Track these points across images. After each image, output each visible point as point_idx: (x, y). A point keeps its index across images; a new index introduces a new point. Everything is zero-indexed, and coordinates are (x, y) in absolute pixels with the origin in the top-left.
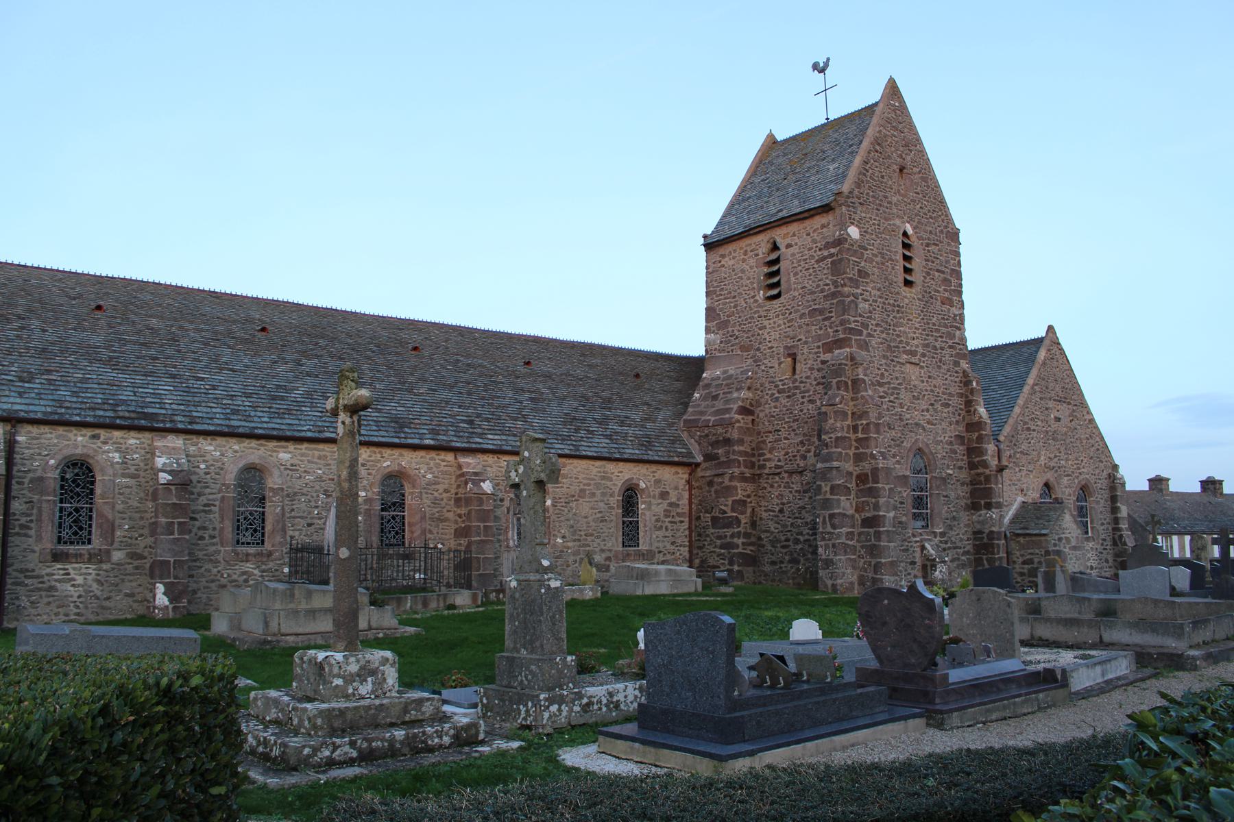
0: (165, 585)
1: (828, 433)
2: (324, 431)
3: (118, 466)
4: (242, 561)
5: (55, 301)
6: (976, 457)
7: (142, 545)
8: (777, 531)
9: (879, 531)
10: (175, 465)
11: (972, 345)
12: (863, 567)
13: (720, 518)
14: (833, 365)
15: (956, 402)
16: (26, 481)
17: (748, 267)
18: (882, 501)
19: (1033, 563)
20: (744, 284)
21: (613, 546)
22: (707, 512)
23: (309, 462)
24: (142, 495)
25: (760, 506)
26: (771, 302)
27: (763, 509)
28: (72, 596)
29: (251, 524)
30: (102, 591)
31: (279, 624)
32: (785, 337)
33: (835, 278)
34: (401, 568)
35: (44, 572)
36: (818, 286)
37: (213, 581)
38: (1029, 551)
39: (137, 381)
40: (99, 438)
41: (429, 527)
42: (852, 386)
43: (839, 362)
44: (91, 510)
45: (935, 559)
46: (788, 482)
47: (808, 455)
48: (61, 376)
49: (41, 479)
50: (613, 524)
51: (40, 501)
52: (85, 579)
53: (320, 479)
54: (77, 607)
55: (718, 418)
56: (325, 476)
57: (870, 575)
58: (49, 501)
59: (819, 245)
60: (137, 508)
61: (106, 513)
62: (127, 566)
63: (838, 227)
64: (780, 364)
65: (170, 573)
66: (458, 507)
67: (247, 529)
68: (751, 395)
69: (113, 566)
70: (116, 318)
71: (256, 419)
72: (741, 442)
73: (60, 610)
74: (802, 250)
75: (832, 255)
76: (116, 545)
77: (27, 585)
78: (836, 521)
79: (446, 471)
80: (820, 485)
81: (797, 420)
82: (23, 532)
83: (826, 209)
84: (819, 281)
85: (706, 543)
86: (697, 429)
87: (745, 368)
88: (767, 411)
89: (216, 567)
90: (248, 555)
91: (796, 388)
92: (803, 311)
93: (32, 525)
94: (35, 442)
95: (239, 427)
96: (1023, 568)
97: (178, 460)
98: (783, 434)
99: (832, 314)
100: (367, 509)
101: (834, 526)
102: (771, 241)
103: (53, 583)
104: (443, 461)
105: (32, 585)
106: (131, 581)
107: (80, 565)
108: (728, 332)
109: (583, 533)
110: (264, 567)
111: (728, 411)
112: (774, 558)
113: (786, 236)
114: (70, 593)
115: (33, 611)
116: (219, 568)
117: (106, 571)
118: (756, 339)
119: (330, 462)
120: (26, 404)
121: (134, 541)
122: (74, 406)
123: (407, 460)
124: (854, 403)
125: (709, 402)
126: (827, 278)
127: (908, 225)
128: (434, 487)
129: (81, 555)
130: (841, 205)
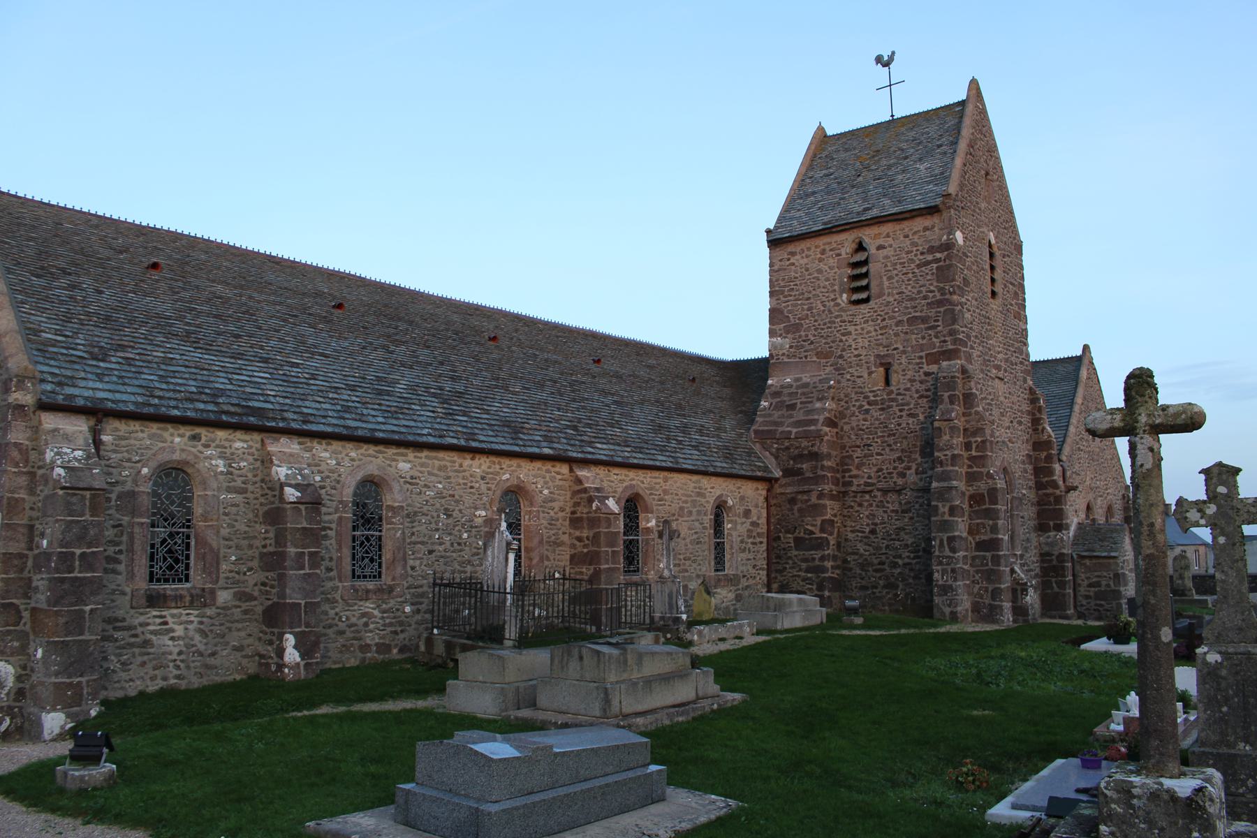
0: (295, 635)
1: (941, 450)
2: (445, 436)
3: (222, 478)
4: (361, 600)
5: (99, 253)
6: (1044, 477)
7: (251, 582)
8: (867, 553)
9: (998, 556)
10: (299, 477)
11: (1033, 359)
12: (978, 593)
13: (807, 539)
14: (944, 378)
15: (1026, 419)
16: (114, 496)
17: (826, 268)
18: (1000, 522)
19: (1100, 586)
20: (822, 285)
21: (706, 571)
22: (788, 532)
23: (429, 473)
24: (251, 516)
25: (845, 526)
26: (858, 307)
27: (849, 529)
28: (171, 654)
29: (367, 552)
30: (206, 644)
31: (620, 702)
32: (877, 345)
33: (942, 285)
34: (520, 603)
35: (136, 622)
36: (919, 292)
37: (330, 626)
38: (1096, 574)
39: (228, 365)
40: (200, 439)
41: (546, 552)
42: (963, 400)
43: (952, 374)
44: (188, 537)
45: (1026, 583)
46: (881, 501)
47: (908, 472)
48: (139, 354)
49: (132, 495)
50: (706, 547)
51: (132, 525)
52: (186, 629)
53: (440, 495)
54: (178, 667)
55: (801, 429)
56: (445, 491)
57: (987, 602)
58: (142, 524)
59: (921, 248)
60: (245, 533)
61: (209, 540)
62: (234, 610)
63: (946, 231)
64: (870, 373)
65: (300, 619)
66: (576, 528)
67: (363, 558)
68: (834, 406)
69: (218, 611)
70: (176, 281)
71: (371, 419)
72: (829, 456)
73: (157, 672)
74: (898, 252)
75: (937, 260)
76: (221, 582)
77: (116, 640)
78: (957, 544)
79: (561, 486)
80: (937, 506)
81: (894, 435)
82: (111, 566)
83: (933, 210)
84: (921, 287)
85: (788, 566)
86: (774, 441)
87: (824, 376)
88: (854, 424)
89: (333, 608)
90: (368, 591)
91: (893, 400)
92: (900, 318)
93: (122, 557)
94: (123, 443)
95: (357, 428)
96: (1089, 591)
97: (301, 470)
98: (875, 449)
99: (939, 323)
100: (487, 532)
101: (953, 550)
102: (857, 241)
103: (149, 636)
104: (558, 473)
105: (123, 639)
106: (239, 630)
107: (180, 610)
108: (800, 336)
109: (682, 557)
110: (384, 606)
111: (814, 422)
112: (864, 583)
113: (877, 236)
114: (168, 649)
115: (123, 675)
116: (337, 610)
117: (210, 618)
118: (839, 346)
119: (450, 474)
120: (110, 391)
121: (242, 578)
122: (167, 395)
123: (526, 472)
124: (967, 418)
125: (784, 412)
126: (931, 284)
127: (991, 234)
128: (550, 504)
129: (181, 597)
130: (949, 208)
